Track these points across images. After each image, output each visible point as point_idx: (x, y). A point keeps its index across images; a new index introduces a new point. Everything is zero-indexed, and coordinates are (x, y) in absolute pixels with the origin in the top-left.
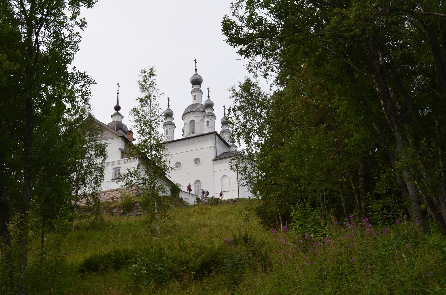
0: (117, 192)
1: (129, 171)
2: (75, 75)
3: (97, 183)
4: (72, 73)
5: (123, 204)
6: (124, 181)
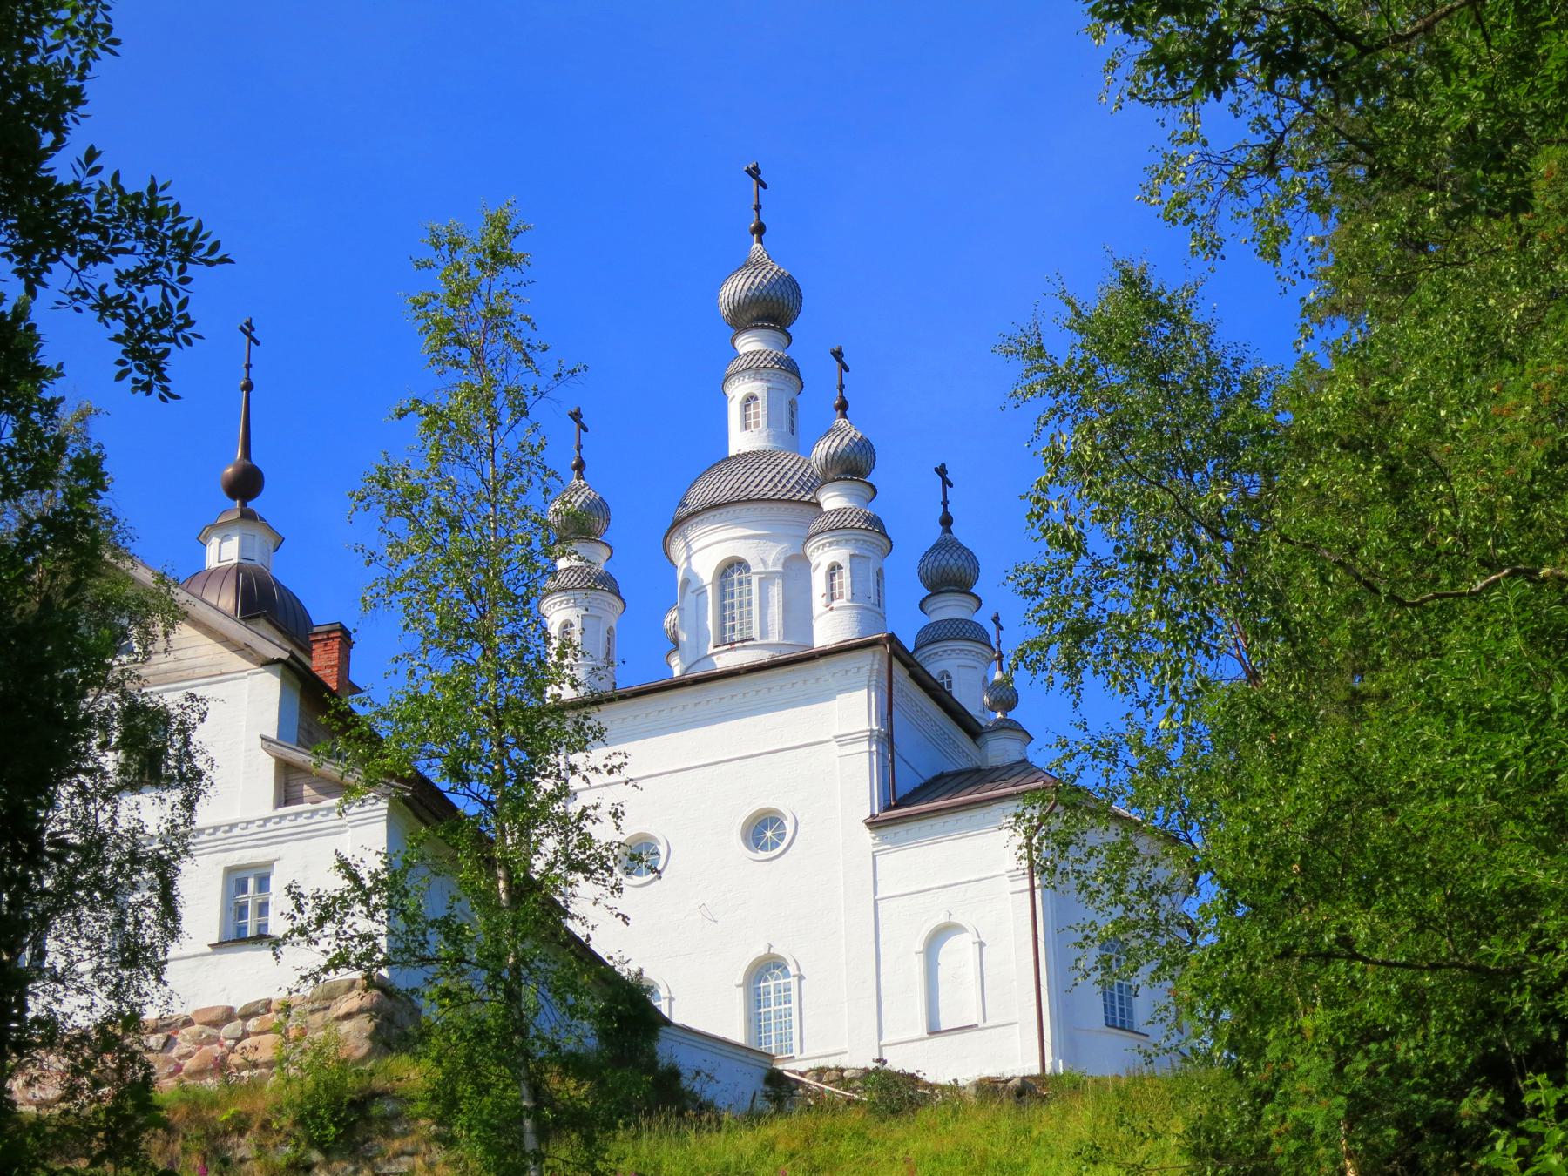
0: (252, 1024)
1: (354, 877)
2: (93, 207)
3: (135, 957)
4: (77, 185)
5: (294, 1093)
6: (323, 944)
